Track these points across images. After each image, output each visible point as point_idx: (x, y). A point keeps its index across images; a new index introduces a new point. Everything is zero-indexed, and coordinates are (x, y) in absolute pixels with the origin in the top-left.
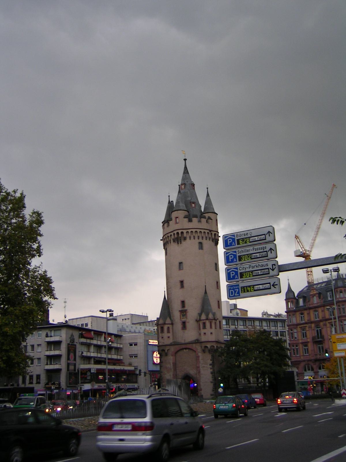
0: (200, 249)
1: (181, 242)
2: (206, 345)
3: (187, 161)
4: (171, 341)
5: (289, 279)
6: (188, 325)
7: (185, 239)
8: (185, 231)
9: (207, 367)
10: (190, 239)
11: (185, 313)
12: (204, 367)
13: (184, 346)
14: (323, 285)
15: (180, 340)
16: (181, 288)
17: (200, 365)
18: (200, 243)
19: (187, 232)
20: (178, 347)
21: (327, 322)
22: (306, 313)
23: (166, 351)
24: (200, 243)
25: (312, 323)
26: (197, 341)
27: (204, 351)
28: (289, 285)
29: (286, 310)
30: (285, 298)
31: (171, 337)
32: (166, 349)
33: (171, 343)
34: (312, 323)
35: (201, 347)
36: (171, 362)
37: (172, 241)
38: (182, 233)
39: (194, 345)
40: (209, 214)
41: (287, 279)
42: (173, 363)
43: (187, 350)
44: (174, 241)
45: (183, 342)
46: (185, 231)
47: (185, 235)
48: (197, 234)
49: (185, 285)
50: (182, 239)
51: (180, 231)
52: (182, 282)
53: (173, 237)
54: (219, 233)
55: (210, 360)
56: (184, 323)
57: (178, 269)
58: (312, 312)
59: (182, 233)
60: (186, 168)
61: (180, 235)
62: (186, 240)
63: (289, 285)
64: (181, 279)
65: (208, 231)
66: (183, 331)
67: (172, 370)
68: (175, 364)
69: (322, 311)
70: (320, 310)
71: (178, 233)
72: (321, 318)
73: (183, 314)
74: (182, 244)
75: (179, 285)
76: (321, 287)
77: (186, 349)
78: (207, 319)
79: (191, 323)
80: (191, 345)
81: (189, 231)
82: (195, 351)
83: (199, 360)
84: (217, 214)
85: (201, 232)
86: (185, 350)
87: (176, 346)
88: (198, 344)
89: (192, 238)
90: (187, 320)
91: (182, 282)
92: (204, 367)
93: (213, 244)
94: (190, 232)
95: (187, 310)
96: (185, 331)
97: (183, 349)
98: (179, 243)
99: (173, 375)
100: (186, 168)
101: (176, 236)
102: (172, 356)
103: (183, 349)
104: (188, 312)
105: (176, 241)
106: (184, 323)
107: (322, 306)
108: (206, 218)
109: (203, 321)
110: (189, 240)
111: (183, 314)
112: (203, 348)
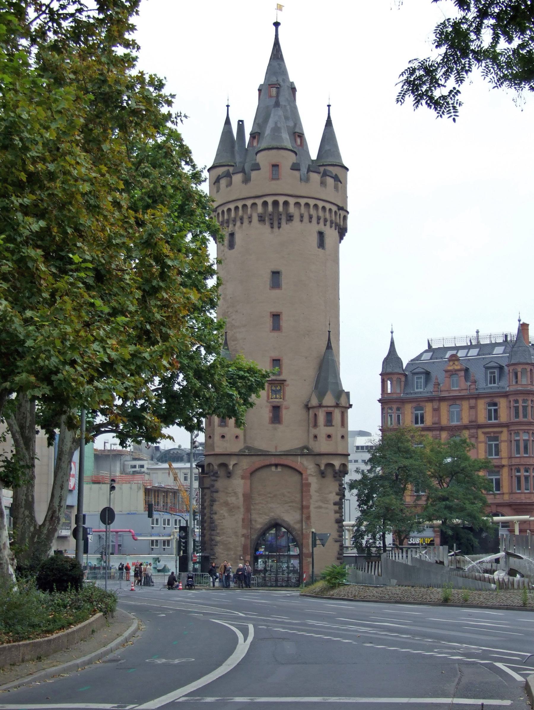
0: (319, 247)
1: (279, 223)
2: (331, 462)
3: (280, 28)
4: (237, 447)
5: (394, 330)
6: (285, 414)
7: (290, 218)
8: (292, 201)
9: (327, 508)
10: (301, 221)
11: (278, 388)
12: (320, 507)
13: (274, 460)
14: (474, 352)
15: (261, 444)
16: (273, 330)
17: (312, 501)
18: (321, 234)
19: (297, 204)
20: (259, 461)
21: (480, 431)
22: (428, 408)
23: (231, 467)
24: (321, 234)
25: (442, 429)
26: (306, 452)
27: (323, 474)
28: (392, 344)
29: (380, 397)
30: (380, 371)
31: (241, 437)
32: (232, 462)
33: (240, 451)
34: (442, 429)
35: (318, 465)
36: (240, 491)
37: (255, 218)
38: (286, 203)
39: (299, 458)
40: (336, 168)
41: (390, 330)
42: (245, 495)
43: (279, 469)
44: (261, 219)
45: (272, 450)
46: (292, 201)
47: (292, 209)
48: (300, 209)
49: (284, 324)
50: (284, 218)
51: (281, 200)
52: (276, 316)
53: (260, 209)
54: (348, 213)
55: (334, 494)
56: (276, 409)
57: (268, 287)
58: (444, 407)
59: (286, 203)
60: (277, 44)
61: (281, 209)
62: (293, 222)
63: (392, 344)
64: (275, 310)
65: (334, 208)
66: (273, 425)
67: (242, 510)
68: (248, 498)
69: (471, 408)
70: (465, 405)
71: (276, 203)
72: (465, 421)
73: (274, 388)
74: (281, 229)
75: (269, 322)
76: (466, 356)
77: (276, 465)
78: (337, 406)
79: (292, 413)
80: (291, 458)
81: (303, 201)
82: (301, 473)
83: (309, 492)
84: (347, 169)
85: (324, 208)
86: (273, 469)
87: (254, 458)
88: (310, 458)
89: (306, 218)
90: (285, 404)
91: (276, 316)
92: (320, 507)
93: (338, 238)
94: (303, 204)
95: (285, 381)
96: (277, 425)
97: (270, 465)
98: (276, 224)
99: (243, 520)
100: (277, 44)
101: (270, 208)
102: (243, 478)
103: (270, 465)
104: (288, 385)
105: (267, 219)
106: (276, 409)
107: (473, 398)
108: (319, 173)
109: (326, 409)
110: (299, 223)
111: (274, 388)
112: (323, 468)
